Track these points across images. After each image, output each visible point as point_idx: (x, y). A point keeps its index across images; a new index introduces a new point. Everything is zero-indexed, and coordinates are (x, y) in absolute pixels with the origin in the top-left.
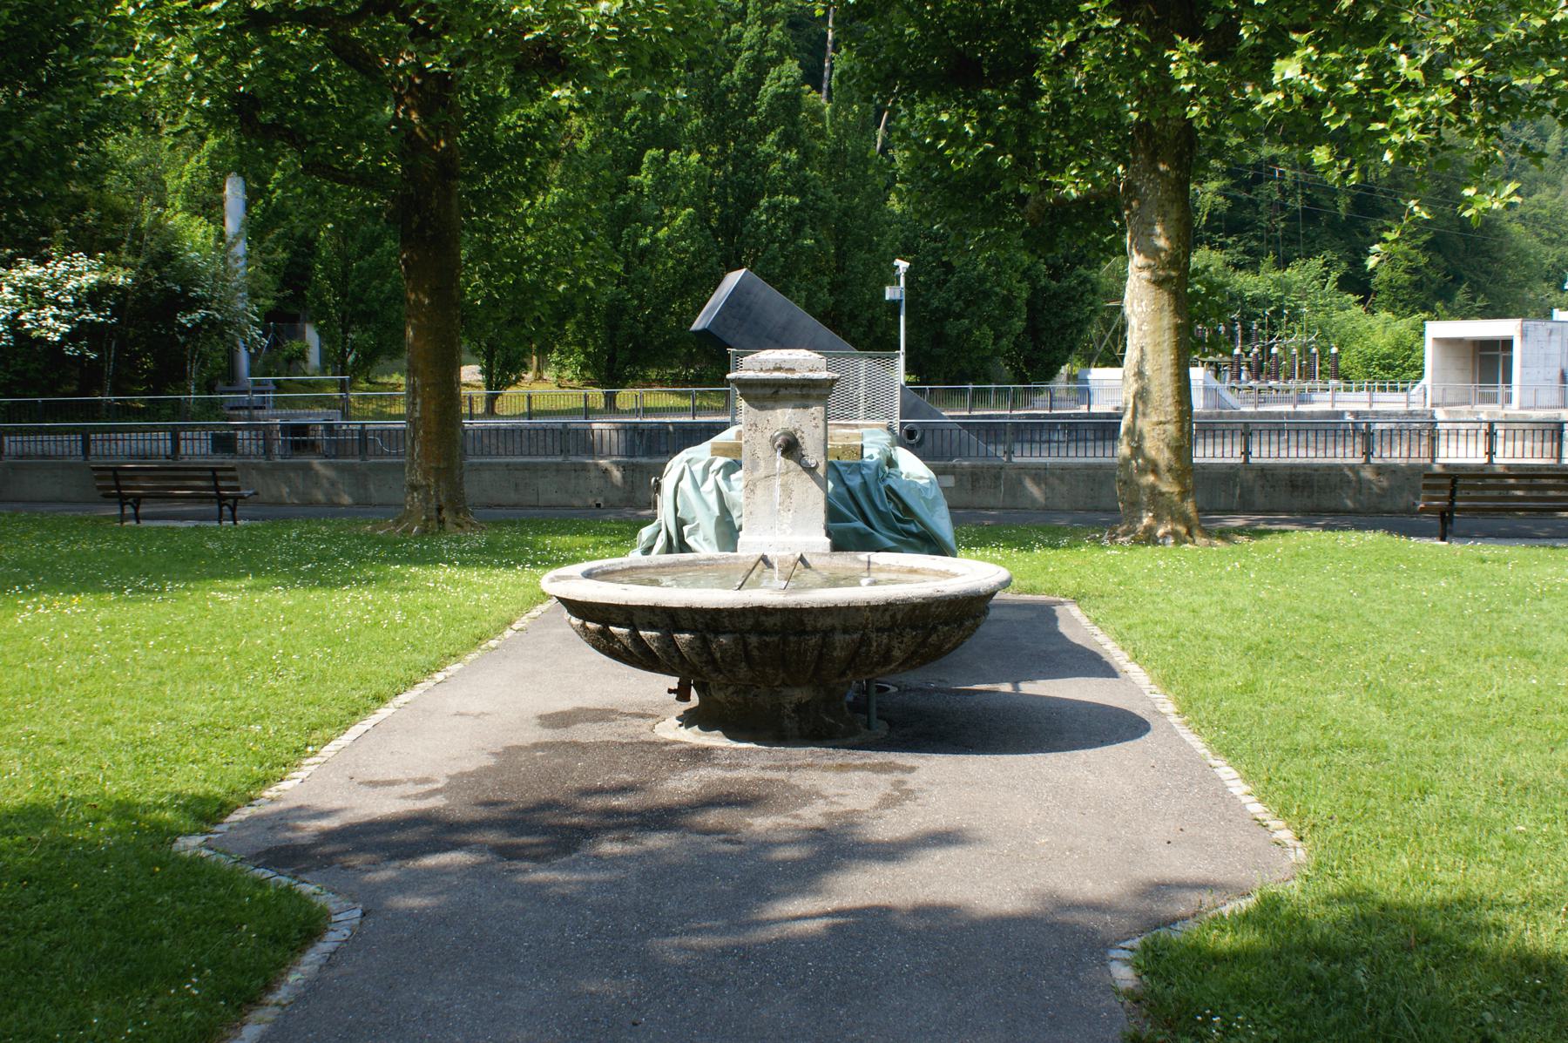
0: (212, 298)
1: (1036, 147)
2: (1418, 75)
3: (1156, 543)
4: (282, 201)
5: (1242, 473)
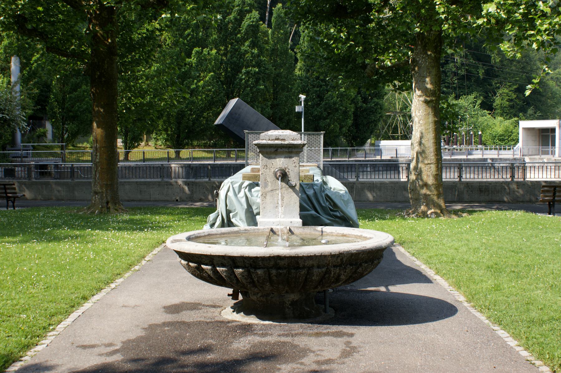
0: (5, 110)
1: (372, 44)
2: (548, 10)
3: (427, 216)
4: (36, 69)
5: (458, 185)
